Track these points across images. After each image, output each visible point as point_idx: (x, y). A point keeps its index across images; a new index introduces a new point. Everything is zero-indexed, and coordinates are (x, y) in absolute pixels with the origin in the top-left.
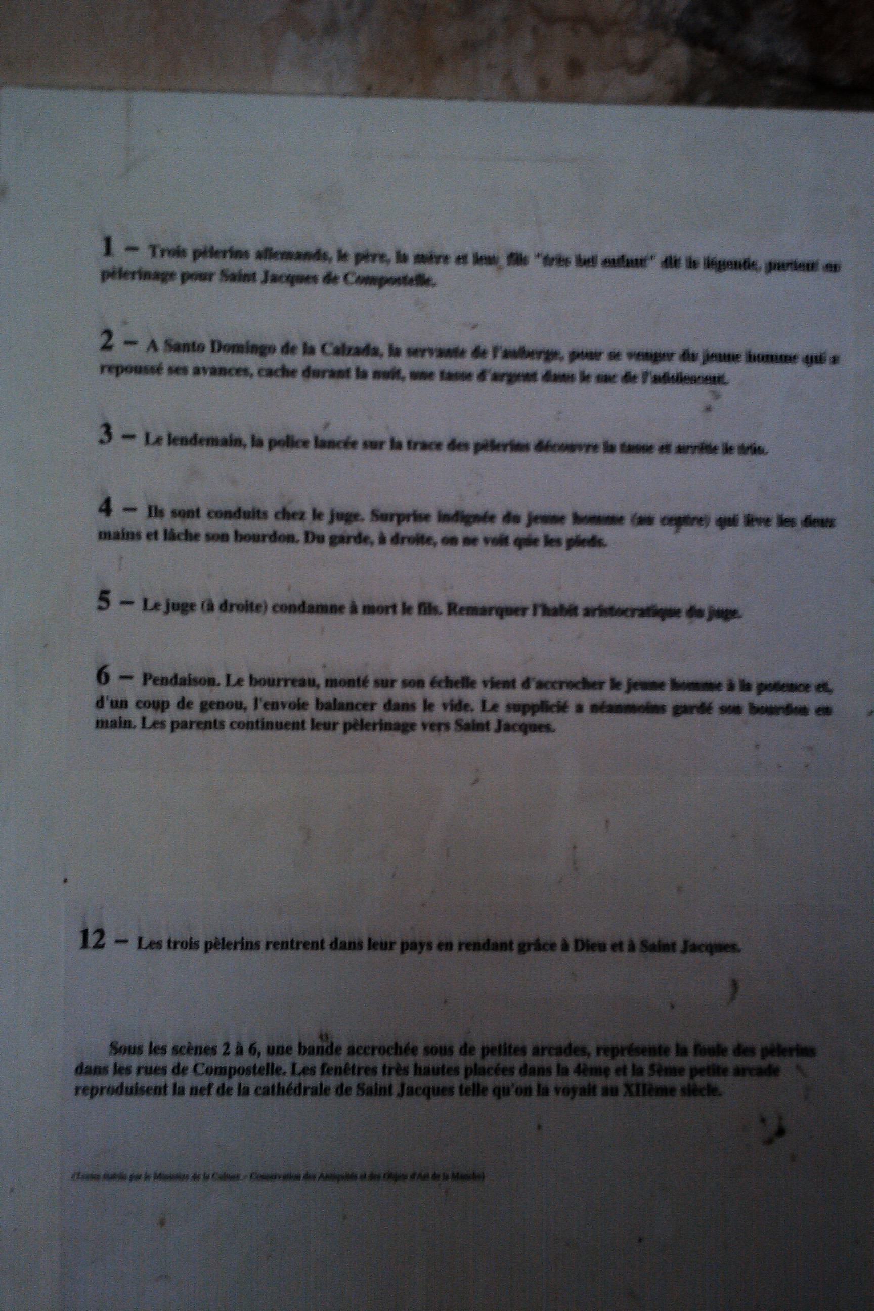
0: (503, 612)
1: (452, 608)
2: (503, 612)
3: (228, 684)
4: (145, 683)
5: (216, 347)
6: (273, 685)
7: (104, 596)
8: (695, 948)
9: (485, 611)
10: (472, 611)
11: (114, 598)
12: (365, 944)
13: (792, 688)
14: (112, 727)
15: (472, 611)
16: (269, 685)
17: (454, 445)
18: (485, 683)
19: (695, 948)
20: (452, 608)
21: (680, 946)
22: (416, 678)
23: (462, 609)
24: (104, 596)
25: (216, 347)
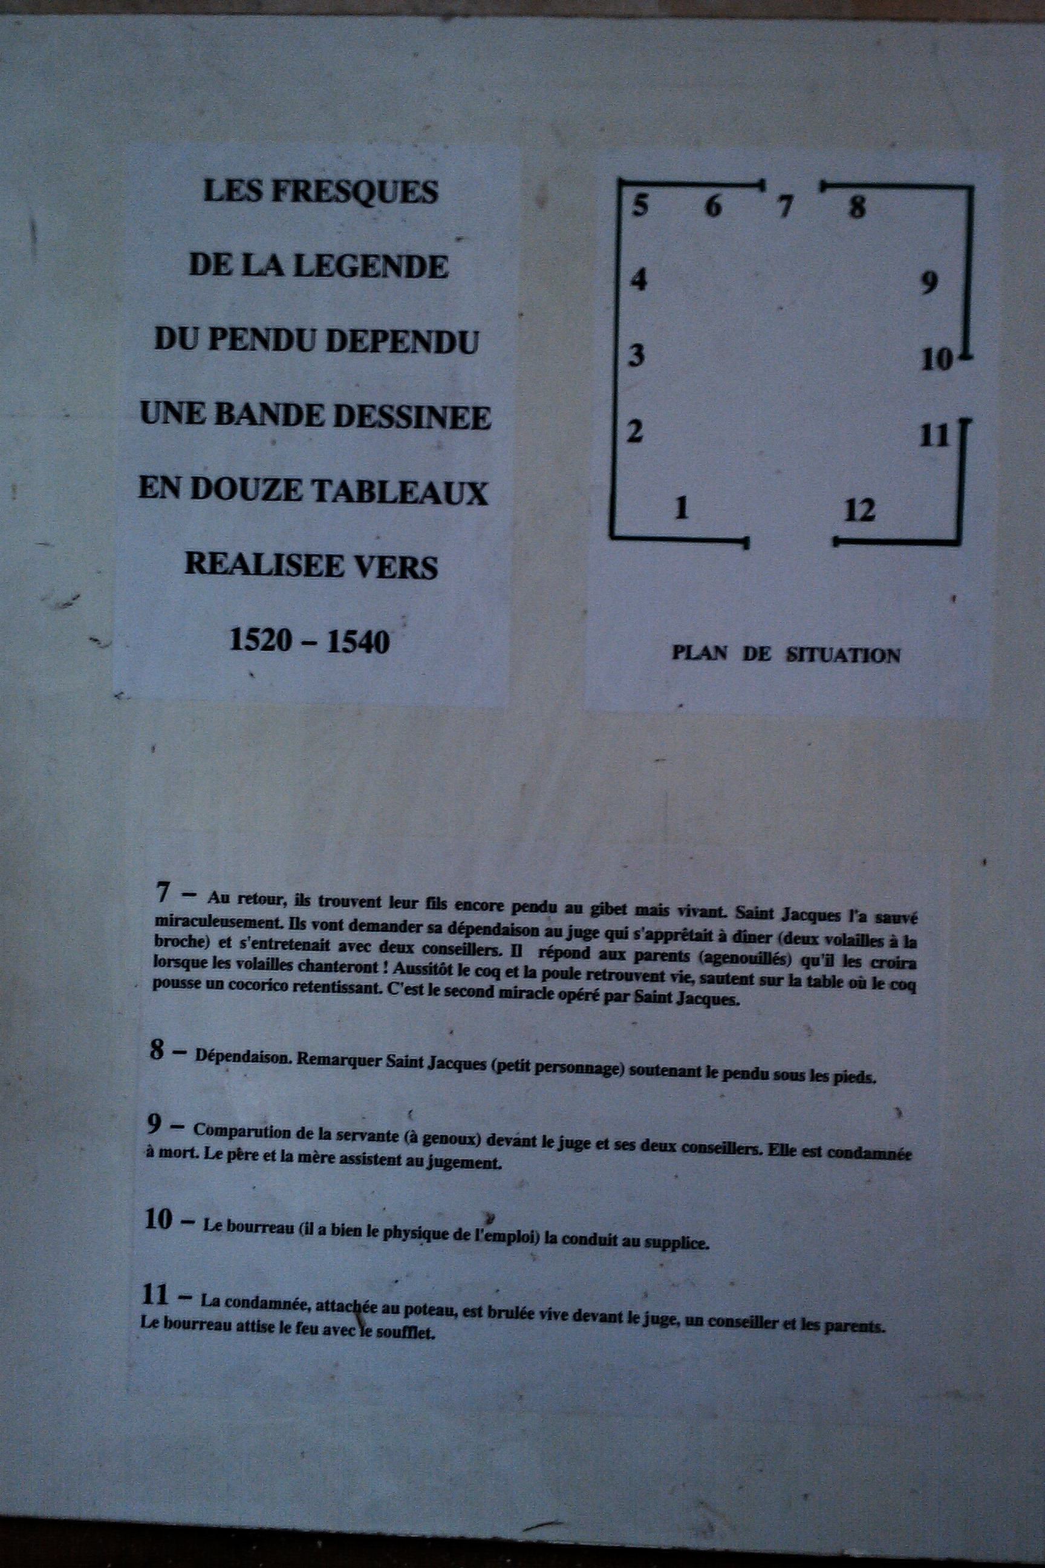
0: (356, 1062)
1: (302, 1058)
2: (356, 1062)
3: (207, 1157)
4: (676, 657)
5: (202, 1055)
6: (189, 1328)
7: (157, 1048)
8: (442, 1065)
9: (337, 1061)
10: (324, 1060)
11: (167, 1049)
12: (807, 1076)
13: (461, 1140)
14: (333, 1064)
15: (324, 1060)
16: (395, 1336)
17: (816, 1077)
18: (681, 911)
19: (442, 1065)
20: (302, 1058)
21: (427, 1062)
22: (279, 1054)
23: (312, 1058)
24: (157, 1048)
25: (202, 1055)
